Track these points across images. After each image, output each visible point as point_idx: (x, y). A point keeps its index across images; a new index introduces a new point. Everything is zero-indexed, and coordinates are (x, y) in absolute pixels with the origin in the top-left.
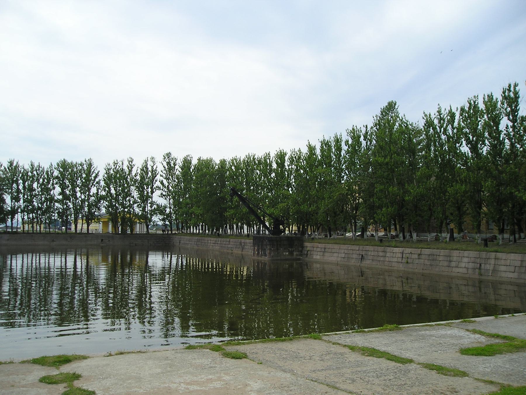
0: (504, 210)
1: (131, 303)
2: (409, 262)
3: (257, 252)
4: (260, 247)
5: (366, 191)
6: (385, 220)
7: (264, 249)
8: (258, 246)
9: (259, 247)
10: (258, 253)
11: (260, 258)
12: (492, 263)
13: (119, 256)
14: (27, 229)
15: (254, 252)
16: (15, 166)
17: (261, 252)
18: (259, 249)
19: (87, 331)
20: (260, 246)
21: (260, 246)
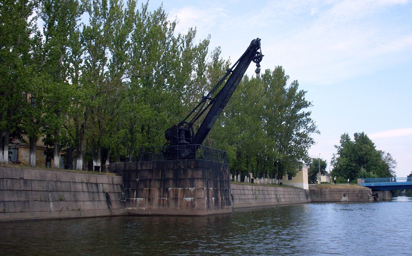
0: (405, 190)
1: (407, 250)
2: (6, 211)
3: (213, 198)
4: (219, 188)
5: (13, 63)
6: (16, 104)
7: (226, 190)
8: (215, 186)
9: (217, 187)
10: (217, 200)
11: (220, 211)
12: (86, 194)
13: (222, 255)
14: (5, 152)
15: (208, 198)
16: (83, 33)
17: (221, 196)
18: (217, 190)
19: (389, 181)
20: (219, 184)
21: (219, 184)
